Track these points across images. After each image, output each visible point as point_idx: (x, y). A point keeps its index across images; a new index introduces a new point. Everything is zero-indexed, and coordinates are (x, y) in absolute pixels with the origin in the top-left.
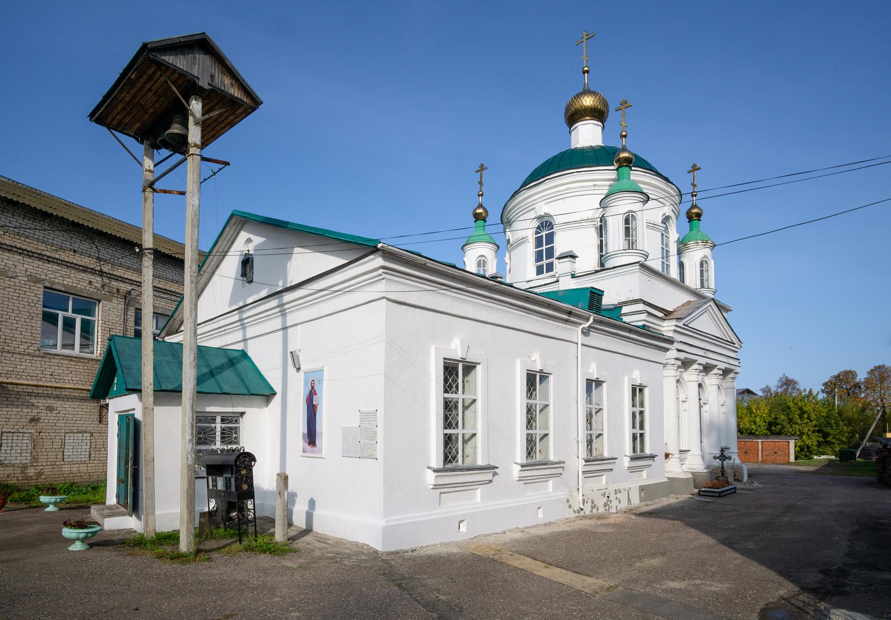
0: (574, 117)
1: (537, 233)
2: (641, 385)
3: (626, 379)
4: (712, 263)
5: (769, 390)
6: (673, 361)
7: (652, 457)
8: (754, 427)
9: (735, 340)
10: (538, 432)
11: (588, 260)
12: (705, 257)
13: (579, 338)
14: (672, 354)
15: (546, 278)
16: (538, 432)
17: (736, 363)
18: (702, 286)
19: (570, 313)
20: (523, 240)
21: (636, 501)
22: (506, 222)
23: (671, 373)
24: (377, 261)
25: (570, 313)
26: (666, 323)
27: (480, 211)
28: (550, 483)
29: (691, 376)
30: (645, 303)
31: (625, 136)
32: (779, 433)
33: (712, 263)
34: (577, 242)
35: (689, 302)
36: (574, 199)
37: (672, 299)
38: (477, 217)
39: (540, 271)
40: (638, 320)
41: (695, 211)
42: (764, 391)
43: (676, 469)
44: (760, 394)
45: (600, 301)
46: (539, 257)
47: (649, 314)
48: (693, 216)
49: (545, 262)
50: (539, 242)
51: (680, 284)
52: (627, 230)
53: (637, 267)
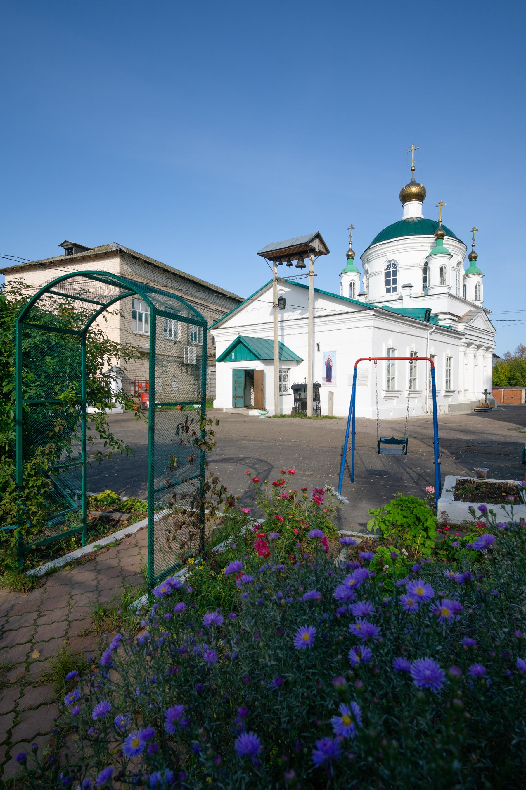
0: (405, 198)
1: (387, 269)
2: (392, 349)
3: (444, 354)
4: (482, 286)
5: (510, 356)
6: (463, 344)
7: (454, 391)
8: (498, 381)
9: (493, 331)
10: (413, 377)
11: (418, 288)
12: (479, 282)
13: (429, 337)
14: (464, 340)
15: (392, 296)
16: (413, 377)
17: (493, 343)
18: (476, 299)
19: (426, 326)
20: (378, 273)
21: (447, 412)
22: (365, 258)
23: (462, 349)
24: (373, 312)
25: (426, 326)
26: (460, 324)
27: (350, 253)
28: (416, 400)
29: (471, 350)
30: (452, 314)
31: (414, 170)
32: (515, 385)
33: (482, 286)
34: (409, 276)
35: (470, 311)
36: (410, 253)
37: (462, 310)
38: (349, 256)
39: (388, 291)
40: (447, 323)
41: (473, 255)
42: (506, 355)
43: (462, 399)
44: (503, 357)
45: (430, 314)
46: (388, 283)
47: (453, 320)
48: (472, 258)
49: (391, 286)
50: (388, 275)
51: (464, 300)
52: (441, 274)
53: (447, 295)
